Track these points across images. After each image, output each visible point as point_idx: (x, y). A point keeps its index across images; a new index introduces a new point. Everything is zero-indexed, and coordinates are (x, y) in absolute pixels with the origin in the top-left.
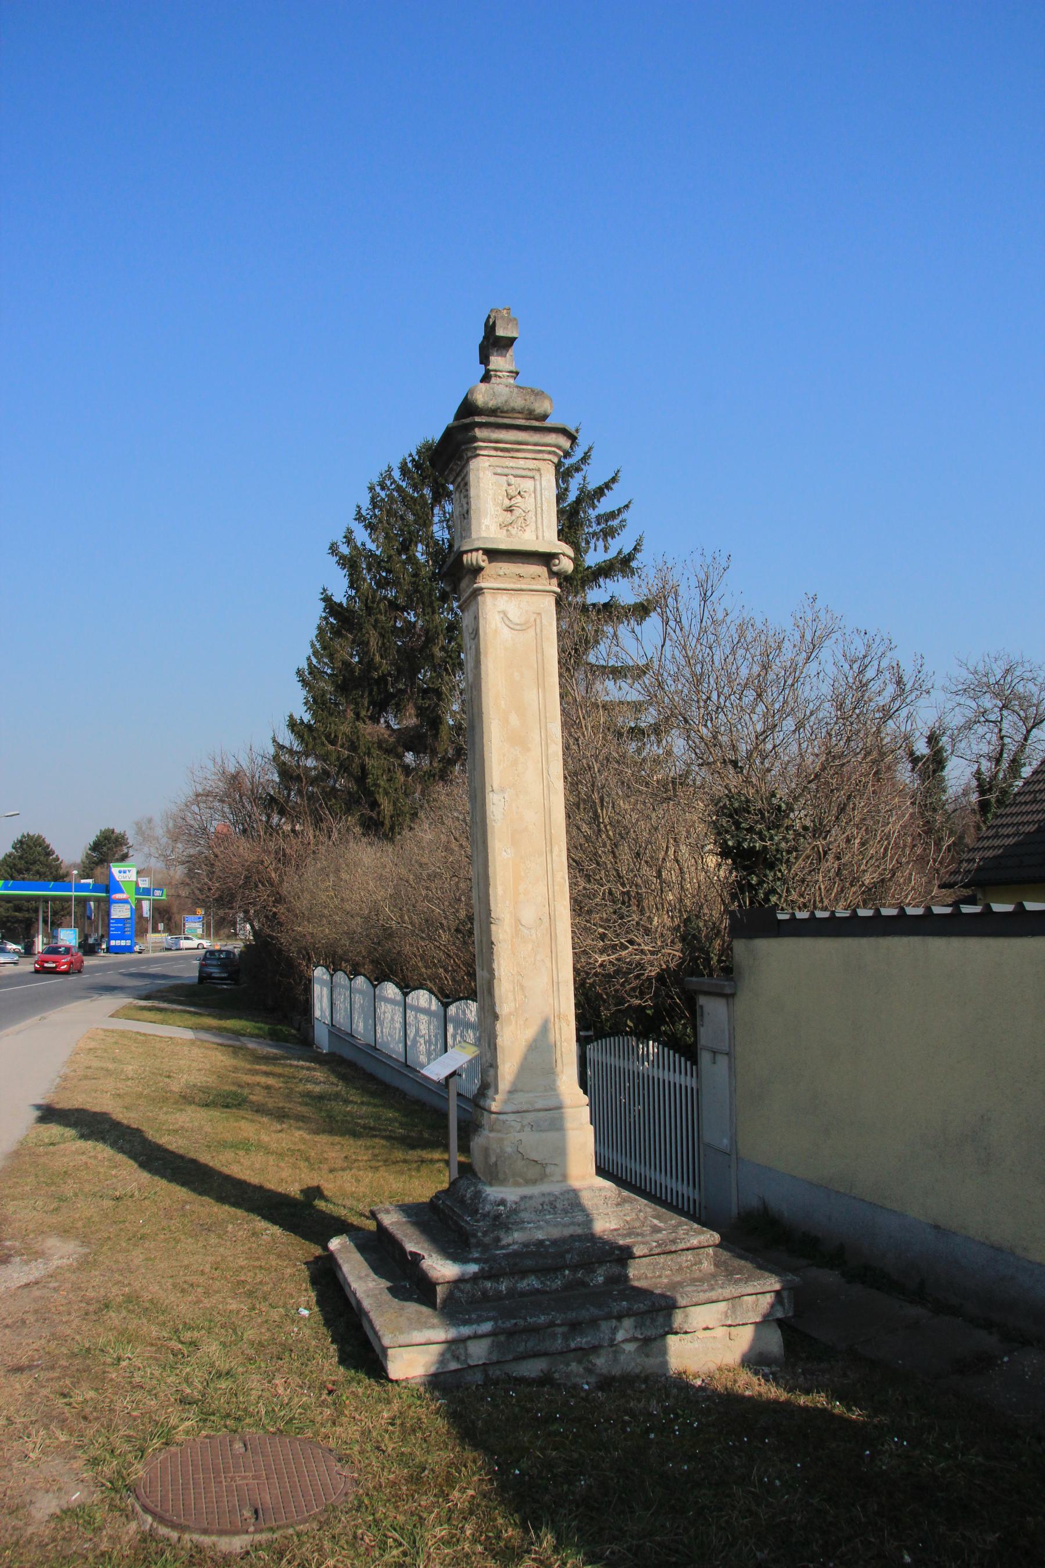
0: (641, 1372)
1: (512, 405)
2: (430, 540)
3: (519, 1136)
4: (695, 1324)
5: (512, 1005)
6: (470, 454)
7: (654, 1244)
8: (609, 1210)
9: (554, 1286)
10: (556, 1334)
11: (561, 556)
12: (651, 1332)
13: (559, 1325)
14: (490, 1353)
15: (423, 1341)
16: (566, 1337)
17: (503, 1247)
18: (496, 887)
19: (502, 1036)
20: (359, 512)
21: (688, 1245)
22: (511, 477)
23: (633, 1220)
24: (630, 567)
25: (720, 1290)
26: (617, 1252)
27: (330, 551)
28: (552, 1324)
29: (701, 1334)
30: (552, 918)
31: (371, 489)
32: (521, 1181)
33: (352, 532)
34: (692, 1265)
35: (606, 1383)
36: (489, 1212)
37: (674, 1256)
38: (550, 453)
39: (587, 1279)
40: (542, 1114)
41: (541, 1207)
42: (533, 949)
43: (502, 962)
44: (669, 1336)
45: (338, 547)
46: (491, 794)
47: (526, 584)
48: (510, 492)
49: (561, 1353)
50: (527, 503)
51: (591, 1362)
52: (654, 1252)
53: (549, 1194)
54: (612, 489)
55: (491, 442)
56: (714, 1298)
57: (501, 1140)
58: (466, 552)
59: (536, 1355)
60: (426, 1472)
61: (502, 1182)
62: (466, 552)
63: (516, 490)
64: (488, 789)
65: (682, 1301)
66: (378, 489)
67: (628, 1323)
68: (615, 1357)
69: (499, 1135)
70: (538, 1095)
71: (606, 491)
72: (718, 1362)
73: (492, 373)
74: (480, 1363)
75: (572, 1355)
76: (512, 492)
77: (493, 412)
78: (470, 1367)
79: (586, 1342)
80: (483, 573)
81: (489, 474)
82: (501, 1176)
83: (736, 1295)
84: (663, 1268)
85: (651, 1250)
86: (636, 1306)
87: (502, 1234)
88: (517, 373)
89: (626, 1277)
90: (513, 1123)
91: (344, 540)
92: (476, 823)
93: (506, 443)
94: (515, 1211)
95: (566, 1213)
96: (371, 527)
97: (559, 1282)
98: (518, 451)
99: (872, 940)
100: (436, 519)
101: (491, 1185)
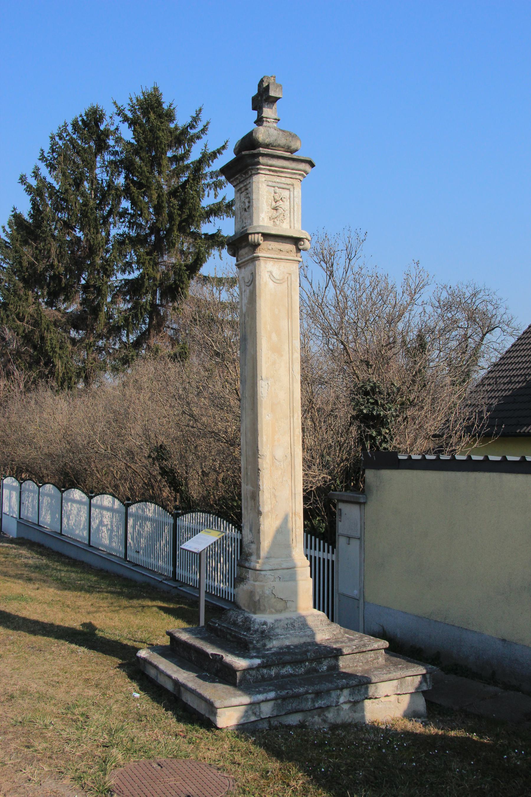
0: (352, 722)
1: (279, 142)
2: (93, 180)
3: (274, 584)
4: (381, 693)
5: (270, 506)
6: (253, 172)
7: (354, 647)
8: (324, 628)
9: (300, 672)
10: (308, 699)
11: (305, 240)
12: (358, 698)
13: (310, 693)
14: (273, 711)
15: (237, 703)
16: (313, 701)
17: (268, 650)
18: (262, 437)
19: (264, 525)
20: (42, 154)
21: (372, 648)
22: (276, 188)
23: (337, 634)
24: (232, 210)
25: (394, 673)
26: (335, 652)
27: (20, 181)
28: (307, 693)
29: (383, 699)
30: (293, 455)
31: (52, 138)
32: (274, 611)
33: (39, 169)
34: (373, 660)
35: (334, 727)
36: (258, 629)
37: (364, 654)
38: (300, 175)
39: (318, 668)
40: (286, 571)
41: (286, 626)
42: (281, 474)
43: (265, 480)
44: (366, 700)
45: (26, 178)
46: (261, 381)
47: (283, 255)
48: (276, 197)
49: (310, 710)
50: (285, 205)
51: (325, 715)
52: (354, 652)
53: (290, 618)
54: (222, 154)
55: (268, 166)
56: (392, 678)
57: (263, 586)
58: (251, 234)
59: (297, 711)
60: (270, 773)
61: (263, 611)
62: (251, 234)
63: (280, 196)
64: (259, 378)
65: (374, 680)
66: (57, 139)
67: (346, 692)
68: (338, 713)
69: (261, 583)
70: (283, 559)
71: (218, 154)
72: (392, 716)
73: (264, 119)
74: (267, 716)
75: (315, 711)
76: (277, 198)
77: (267, 146)
78: (262, 719)
79: (324, 704)
80: (260, 247)
81: (264, 185)
82: (262, 608)
83: (403, 676)
84: (358, 661)
85: (353, 650)
86: (351, 682)
87: (267, 642)
88: (279, 120)
89: (338, 666)
90: (270, 576)
91: (33, 175)
92: (246, 398)
93: (276, 167)
94: (272, 629)
95: (301, 629)
96: (52, 167)
97: (303, 670)
98: (282, 172)
99: (465, 474)
100: (98, 165)
101: (255, 613)
